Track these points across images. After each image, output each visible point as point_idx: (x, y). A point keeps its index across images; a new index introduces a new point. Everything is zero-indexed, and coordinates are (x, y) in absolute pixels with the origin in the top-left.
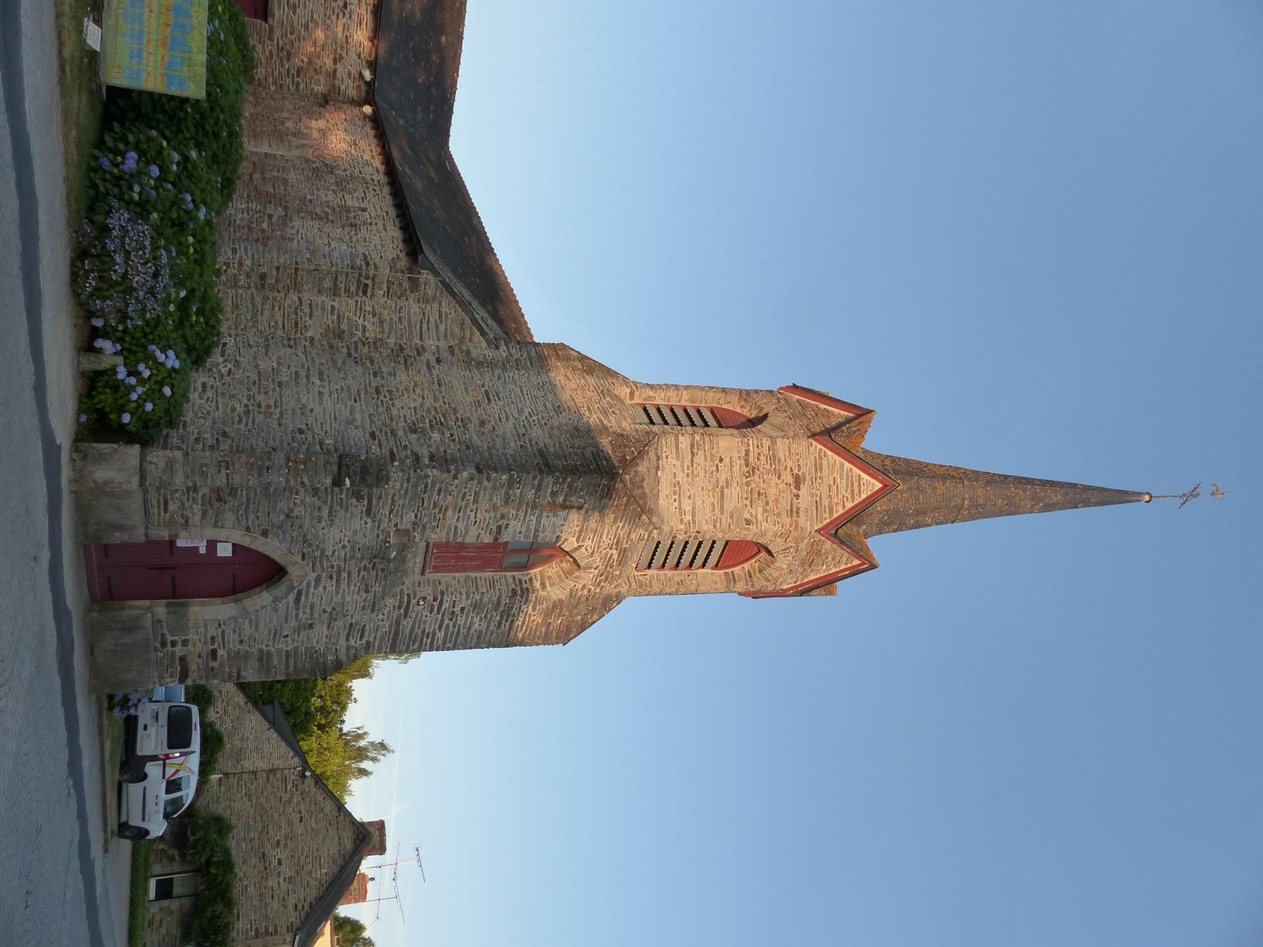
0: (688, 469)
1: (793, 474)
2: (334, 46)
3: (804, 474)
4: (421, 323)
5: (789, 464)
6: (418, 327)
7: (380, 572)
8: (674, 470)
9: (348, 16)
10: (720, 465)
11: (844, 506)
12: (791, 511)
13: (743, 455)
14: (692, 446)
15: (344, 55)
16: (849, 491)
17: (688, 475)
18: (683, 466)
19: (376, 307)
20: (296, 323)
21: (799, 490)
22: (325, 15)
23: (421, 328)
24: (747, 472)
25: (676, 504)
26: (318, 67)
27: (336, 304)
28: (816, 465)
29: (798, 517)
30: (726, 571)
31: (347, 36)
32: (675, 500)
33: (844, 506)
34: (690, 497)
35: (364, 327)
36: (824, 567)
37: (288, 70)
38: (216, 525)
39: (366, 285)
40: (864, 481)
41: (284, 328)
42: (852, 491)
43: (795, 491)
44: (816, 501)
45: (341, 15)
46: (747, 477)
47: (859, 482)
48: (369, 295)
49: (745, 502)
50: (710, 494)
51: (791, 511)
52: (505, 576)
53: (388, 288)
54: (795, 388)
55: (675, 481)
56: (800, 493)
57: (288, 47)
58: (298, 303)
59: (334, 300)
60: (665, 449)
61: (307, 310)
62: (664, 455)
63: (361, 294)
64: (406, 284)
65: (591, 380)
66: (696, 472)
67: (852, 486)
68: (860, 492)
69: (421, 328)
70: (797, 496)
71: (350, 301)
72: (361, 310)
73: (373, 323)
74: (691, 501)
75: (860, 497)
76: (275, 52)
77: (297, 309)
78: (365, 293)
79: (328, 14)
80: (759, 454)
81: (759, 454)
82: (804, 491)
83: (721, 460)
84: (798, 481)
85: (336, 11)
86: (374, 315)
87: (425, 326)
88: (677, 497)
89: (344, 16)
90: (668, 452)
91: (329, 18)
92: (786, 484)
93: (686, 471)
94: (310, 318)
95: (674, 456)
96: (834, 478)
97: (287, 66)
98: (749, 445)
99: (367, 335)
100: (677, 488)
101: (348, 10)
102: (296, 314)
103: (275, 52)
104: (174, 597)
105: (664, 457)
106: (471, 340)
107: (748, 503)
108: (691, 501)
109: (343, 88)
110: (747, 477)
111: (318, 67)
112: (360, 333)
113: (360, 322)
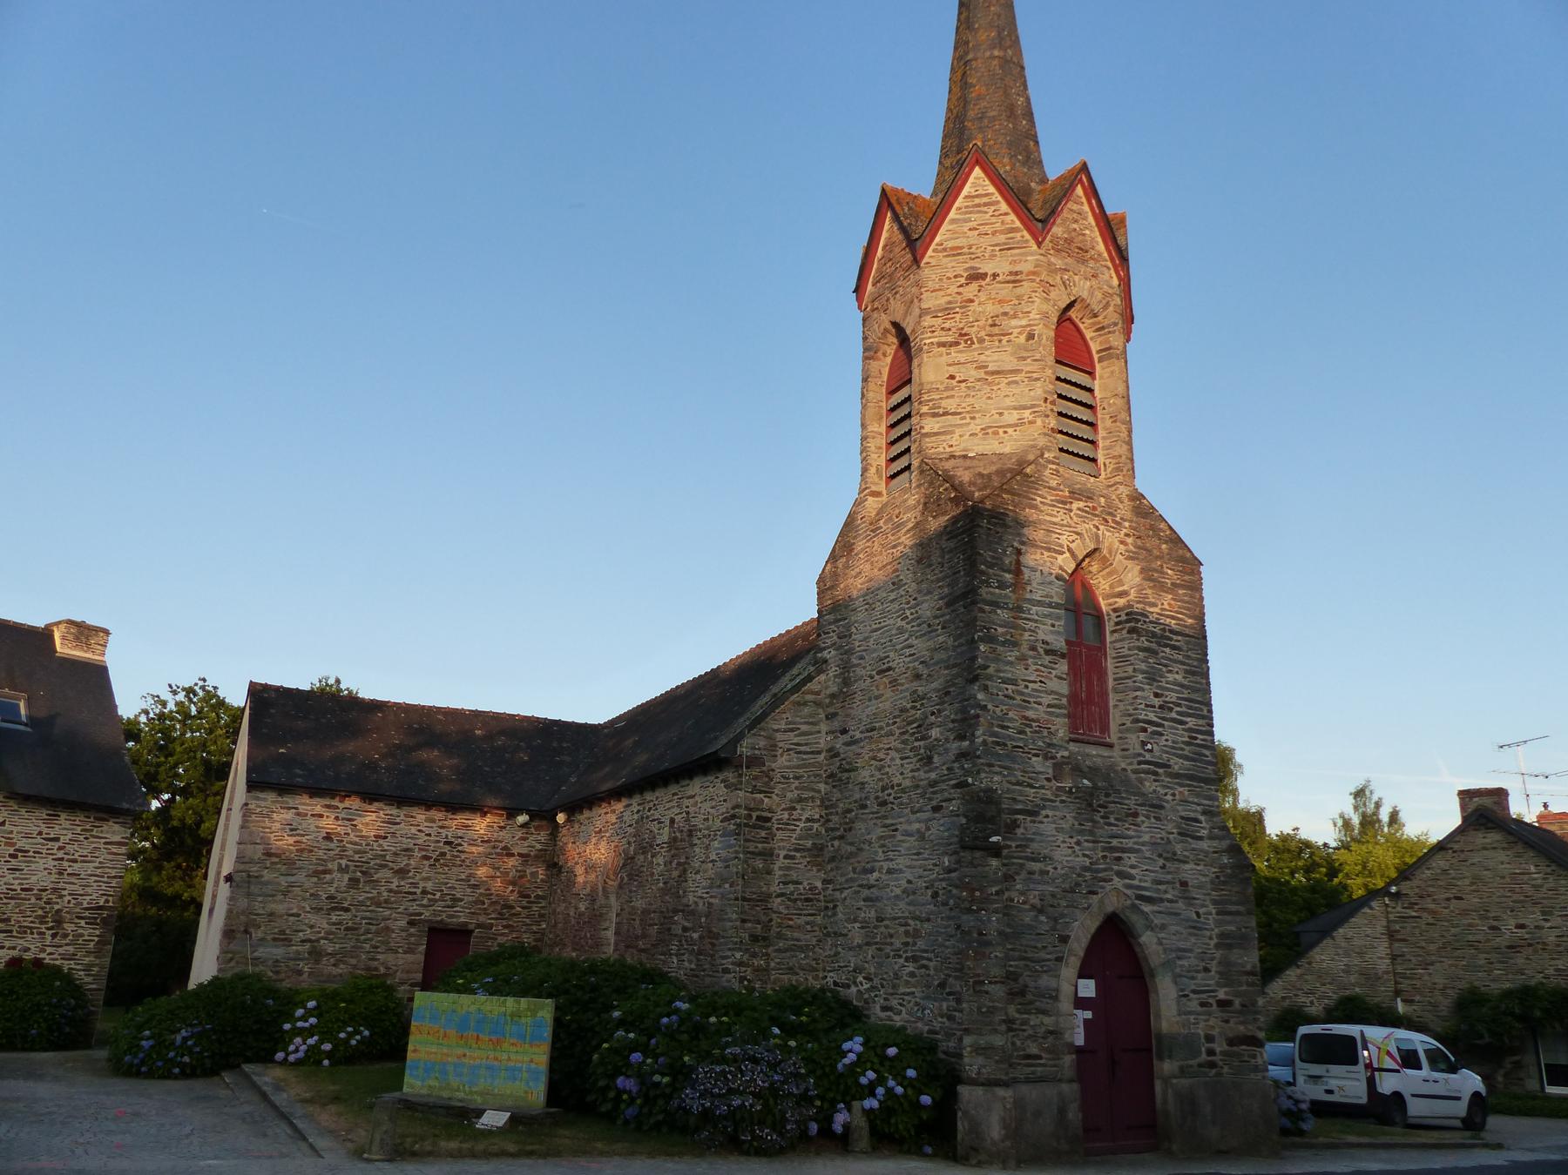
0: (964, 418)
1: (967, 284)
2: (494, 856)
3: (966, 270)
4: (800, 753)
11: (1006, 214)
13: (944, 349)
14: (935, 415)
16: (985, 209)
19: (783, 806)
27: (783, 853)
28: (954, 255)
29: (1021, 273)
31: (482, 842)
33: (1006, 214)
35: (808, 820)
39: (758, 818)
40: (973, 190)
42: (986, 205)
43: (988, 279)
44: (1000, 250)
45: (460, 848)
46: (973, 343)
48: (770, 815)
49: (1004, 342)
54: (859, 290)
57: (499, 908)
61: (791, 887)
62: (948, 450)
63: (770, 824)
65: (860, 545)
66: (968, 409)
68: (987, 195)
70: (995, 276)
71: (778, 837)
72: (788, 824)
73: (803, 809)
74: (1006, 412)
75: (992, 194)
76: (505, 923)
77: (789, 899)
78: (768, 820)
80: (942, 329)
81: (942, 329)
82: (988, 268)
83: (952, 377)
84: (975, 276)
88: (1001, 431)
91: (463, 861)
93: (968, 420)
95: (948, 437)
99: (817, 816)
100: (990, 431)
102: (796, 900)
103: (505, 923)
105: (951, 449)
108: (1006, 412)
110: (973, 343)
112: (816, 825)
113: (802, 825)
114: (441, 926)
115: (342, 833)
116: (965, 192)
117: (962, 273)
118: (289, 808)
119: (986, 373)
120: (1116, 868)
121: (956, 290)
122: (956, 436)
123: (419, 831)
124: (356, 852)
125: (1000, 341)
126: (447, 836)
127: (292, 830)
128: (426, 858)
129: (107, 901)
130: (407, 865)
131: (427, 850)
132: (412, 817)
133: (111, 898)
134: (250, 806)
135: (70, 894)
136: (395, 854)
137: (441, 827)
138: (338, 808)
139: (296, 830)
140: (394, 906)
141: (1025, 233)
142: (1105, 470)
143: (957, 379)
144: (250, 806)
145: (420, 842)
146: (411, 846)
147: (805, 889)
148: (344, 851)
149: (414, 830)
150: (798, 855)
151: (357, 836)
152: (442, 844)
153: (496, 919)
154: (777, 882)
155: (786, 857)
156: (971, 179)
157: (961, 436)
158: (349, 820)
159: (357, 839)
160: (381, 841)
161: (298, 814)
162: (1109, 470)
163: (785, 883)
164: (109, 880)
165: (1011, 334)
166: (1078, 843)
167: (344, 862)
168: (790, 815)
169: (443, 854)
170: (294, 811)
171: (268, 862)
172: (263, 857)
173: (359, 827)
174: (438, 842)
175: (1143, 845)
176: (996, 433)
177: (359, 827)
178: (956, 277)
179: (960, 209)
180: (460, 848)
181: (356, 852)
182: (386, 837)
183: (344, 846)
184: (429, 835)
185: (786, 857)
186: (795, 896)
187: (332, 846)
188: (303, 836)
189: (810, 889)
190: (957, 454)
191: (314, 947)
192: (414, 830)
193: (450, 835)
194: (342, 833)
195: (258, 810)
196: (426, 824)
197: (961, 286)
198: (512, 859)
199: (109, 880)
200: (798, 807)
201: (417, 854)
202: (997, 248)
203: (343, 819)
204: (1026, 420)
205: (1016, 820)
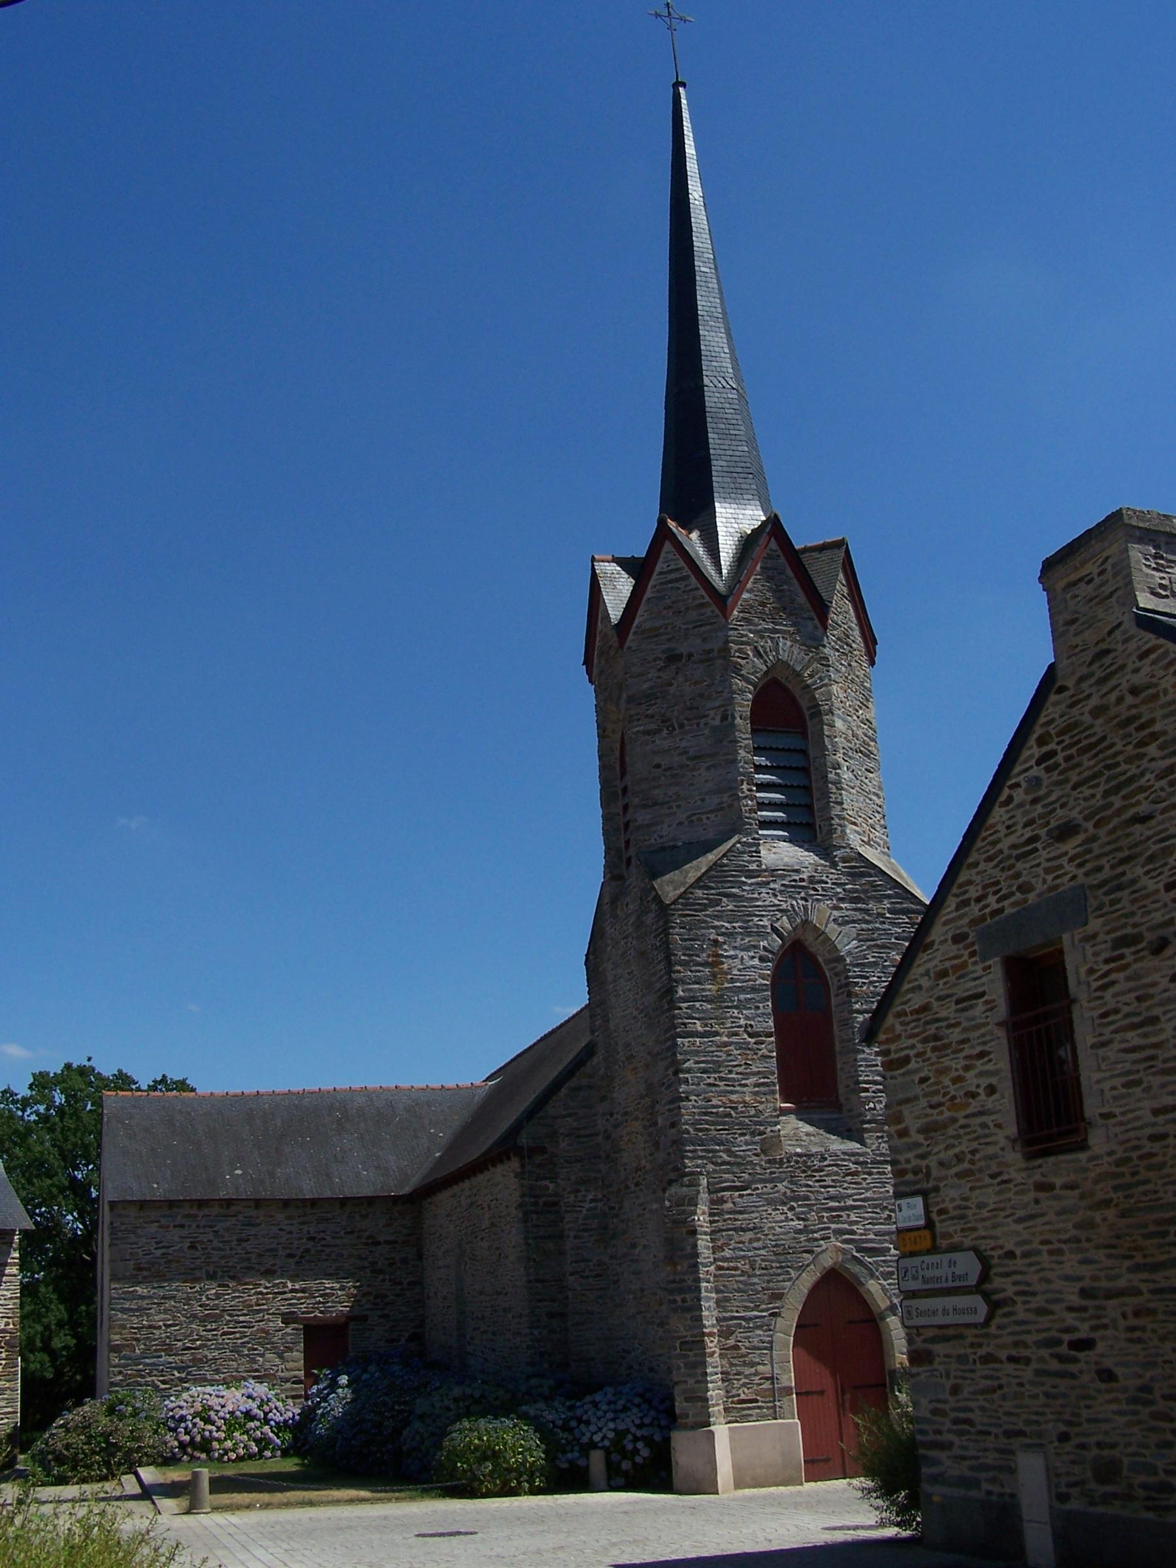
0: (671, 807)
1: (665, 667)
2: (360, 1247)
3: (664, 652)
4: (579, 1136)
5: (653, 674)
6: (584, 1140)
7: (825, 1163)
8: (675, 826)
9: (322, 1235)
10: (663, 767)
11: (696, 589)
12: (707, 660)
13: (649, 737)
14: (645, 806)
15: (367, 1233)
16: (677, 585)
17: (678, 806)
18: (669, 815)
19: (569, 1189)
20: (598, 1276)
21: (682, 655)
22: (327, 1260)
23: (584, 1136)
24: (668, 730)
25: (712, 816)
26: (387, 1262)
27: (572, 1234)
28: (652, 637)
29: (712, 650)
30: (807, 718)
31: (346, 1233)
32: (708, 818)
33: (696, 589)
34: (703, 800)
35: (592, 1201)
36: (785, 587)
37: (397, 1295)
38: (720, 1354)
39: (545, 1204)
40: (665, 566)
41: (604, 1289)
42: (677, 580)
43: (684, 660)
44: (694, 628)
45: (323, 1242)
46: (674, 729)
47: (665, 573)
48: (556, 1199)
49: (701, 725)
50: (696, 773)
51: (707, 660)
52: (837, 1006)
53: (545, 1178)
54: (588, 662)
55: (686, 822)
56: (685, 654)
57: (371, 1298)
58: (577, 1276)
59: (568, 1237)
60: (653, 841)
61: (582, 1265)
62: (659, 841)
63: (557, 1208)
64: (538, 1159)
65: (609, 931)
66: (674, 797)
67: (671, 582)
68: (676, 570)
69: (584, 1136)
70: (690, 655)
71: (567, 1220)
72: (575, 1206)
73: (587, 1191)
74: (707, 797)
75: (683, 568)
76: (380, 1313)
77: (582, 1277)
78: (555, 1204)
79: (325, 1257)
80: (647, 716)
81: (647, 716)
82: (683, 649)
83: (658, 766)
84: (673, 658)
85: (320, 1248)
86: (578, 1191)
87: (582, 1132)
88: (704, 817)
89: (324, 1239)
90: (656, 836)
91: (328, 1255)
92: (677, 674)
93: (675, 809)
94: (590, 1261)
95: (659, 828)
96: (665, 608)
97: (392, 1297)
98: (638, 731)
99: (600, 1196)
100: (694, 818)
101: (315, 1235)
102: (587, 1277)
103: (380, 1313)
104: (884, 1385)
105: (661, 841)
106: (591, 1076)
107: (703, 721)
108: (707, 797)
109: (405, 1231)
110: (674, 729)
111: (387, 1262)
112: (600, 1205)
113: (587, 1205)
114: (314, 1323)
115: (206, 1240)
116: (658, 569)
117: (660, 655)
118: (153, 1222)
119: (688, 759)
120: (833, 1226)
121: (656, 675)
122: (665, 826)
123: (281, 1230)
124: (222, 1257)
125: (698, 724)
126: (309, 1232)
127: (157, 1243)
128: (290, 1256)
129: (7, 1324)
130: (274, 1265)
131: (291, 1248)
132: (271, 1216)
133: (10, 1320)
134: (115, 1225)
135: (1159, 777)
136: (260, 1255)
137: (303, 1223)
138: (197, 1216)
139: (161, 1242)
140: (265, 1307)
141: (714, 608)
142: (821, 833)
143: (663, 767)
144: (115, 1225)
145: (283, 1240)
146: (274, 1246)
147: (594, 1265)
148: (210, 1258)
149: (275, 1229)
150: (586, 1234)
151: (221, 1242)
152: (304, 1240)
153: (372, 1310)
154: (569, 1261)
155: (575, 1237)
156: (663, 554)
157: (669, 826)
158: (211, 1227)
159: (221, 1245)
160: (244, 1244)
161: (161, 1227)
162: (824, 833)
163: (576, 1262)
164: (7, 1302)
165: (707, 716)
166: (792, 1209)
167: (211, 1269)
168: (576, 1197)
169: (307, 1250)
170: (156, 1224)
171: (140, 1277)
172: (134, 1272)
173: (221, 1232)
174: (301, 1239)
175: (852, 1206)
176: (700, 820)
177: (221, 1232)
178: (655, 660)
179: (655, 586)
180: (323, 1242)
181: (222, 1257)
182: (248, 1240)
183: (209, 1253)
184: (290, 1233)
185: (575, 1237)
186: (587, 1273)
187: (197, 1254)
188: (169, 1247)
189: (599, 1265)
190: (667, 845)
191: (26, 1347)
192: (275, 1229)
193: (312, 1230)
194: (206, 1240)
195: (123, 1228)
196: (286, 1222)
197: (659, 670)
198: (379, 1247)
199: (7, 1302)
200: (583, 1189)
201: (281, 1252)
202: (691, 626)
203: (205, 1226)
204: (725, 805)
205: (723, 1196)
